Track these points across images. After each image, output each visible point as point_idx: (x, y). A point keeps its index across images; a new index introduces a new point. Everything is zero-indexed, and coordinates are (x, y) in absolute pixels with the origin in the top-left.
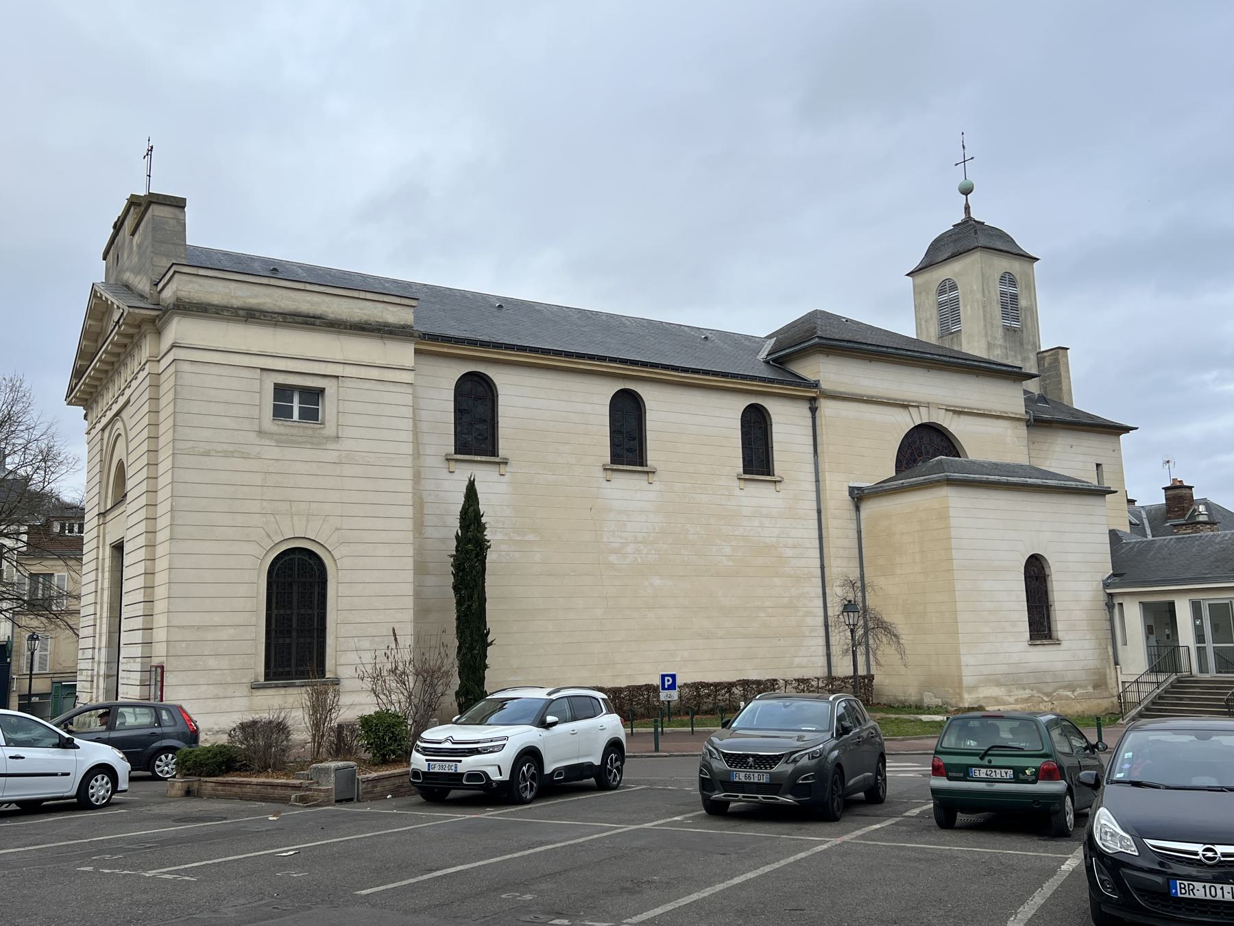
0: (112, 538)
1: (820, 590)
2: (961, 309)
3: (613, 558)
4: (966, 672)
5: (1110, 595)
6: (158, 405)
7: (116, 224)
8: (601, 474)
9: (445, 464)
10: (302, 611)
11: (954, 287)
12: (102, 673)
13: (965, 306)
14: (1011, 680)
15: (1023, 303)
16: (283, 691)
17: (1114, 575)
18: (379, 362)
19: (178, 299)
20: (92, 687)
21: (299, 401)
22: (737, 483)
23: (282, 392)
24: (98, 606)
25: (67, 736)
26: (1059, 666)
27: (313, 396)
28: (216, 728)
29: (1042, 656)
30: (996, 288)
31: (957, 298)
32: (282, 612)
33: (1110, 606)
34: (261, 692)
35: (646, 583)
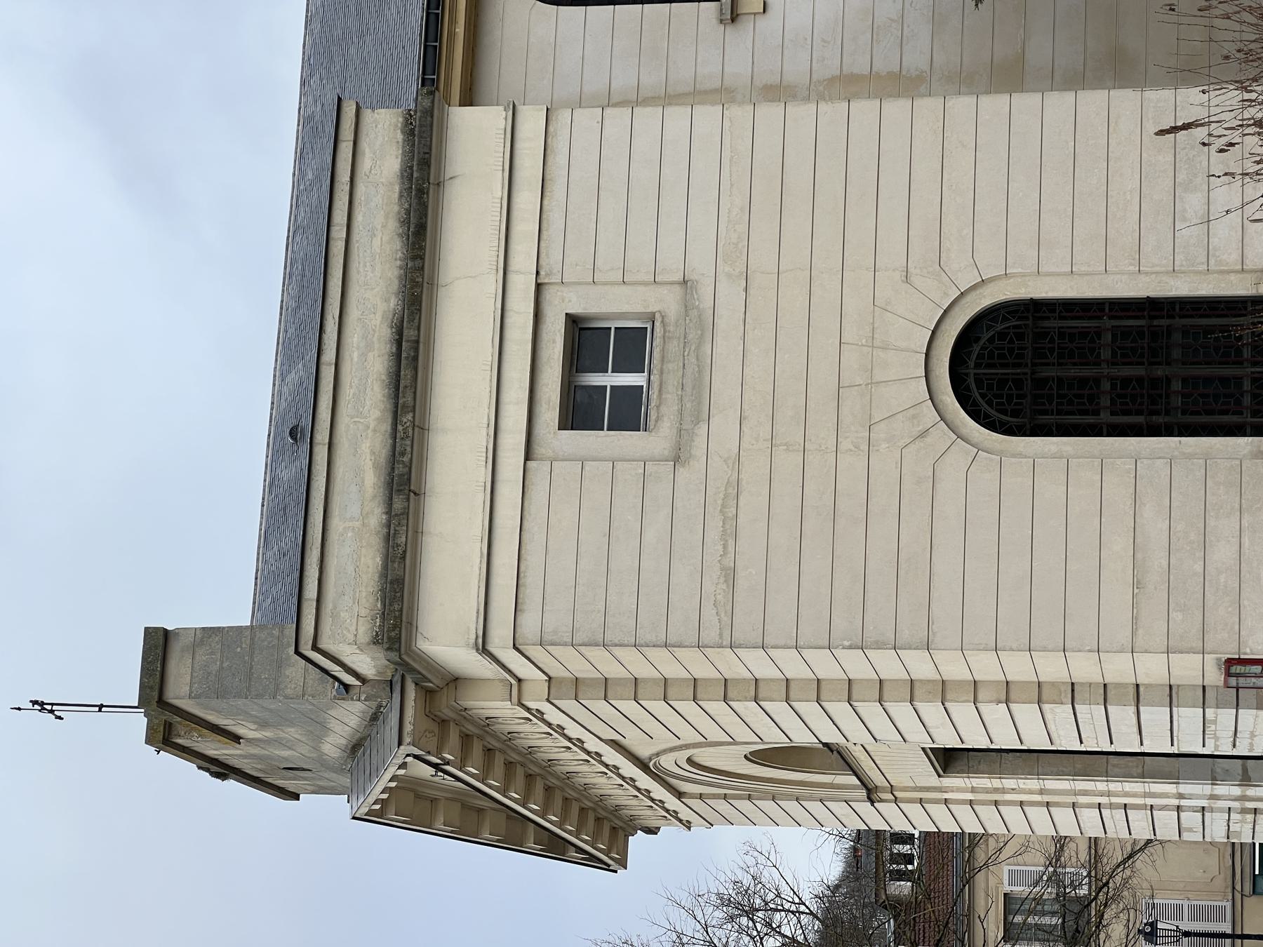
6: (619, 681)
9: (746, 25)
10: (1106, 354)
12: (1236, 791)
18: (499, 191)
19: (376, 641)
21: (599, 373)
23: (580, 411)
24: (1082, 800)
27: (586, 343)
32: (1105, 401)
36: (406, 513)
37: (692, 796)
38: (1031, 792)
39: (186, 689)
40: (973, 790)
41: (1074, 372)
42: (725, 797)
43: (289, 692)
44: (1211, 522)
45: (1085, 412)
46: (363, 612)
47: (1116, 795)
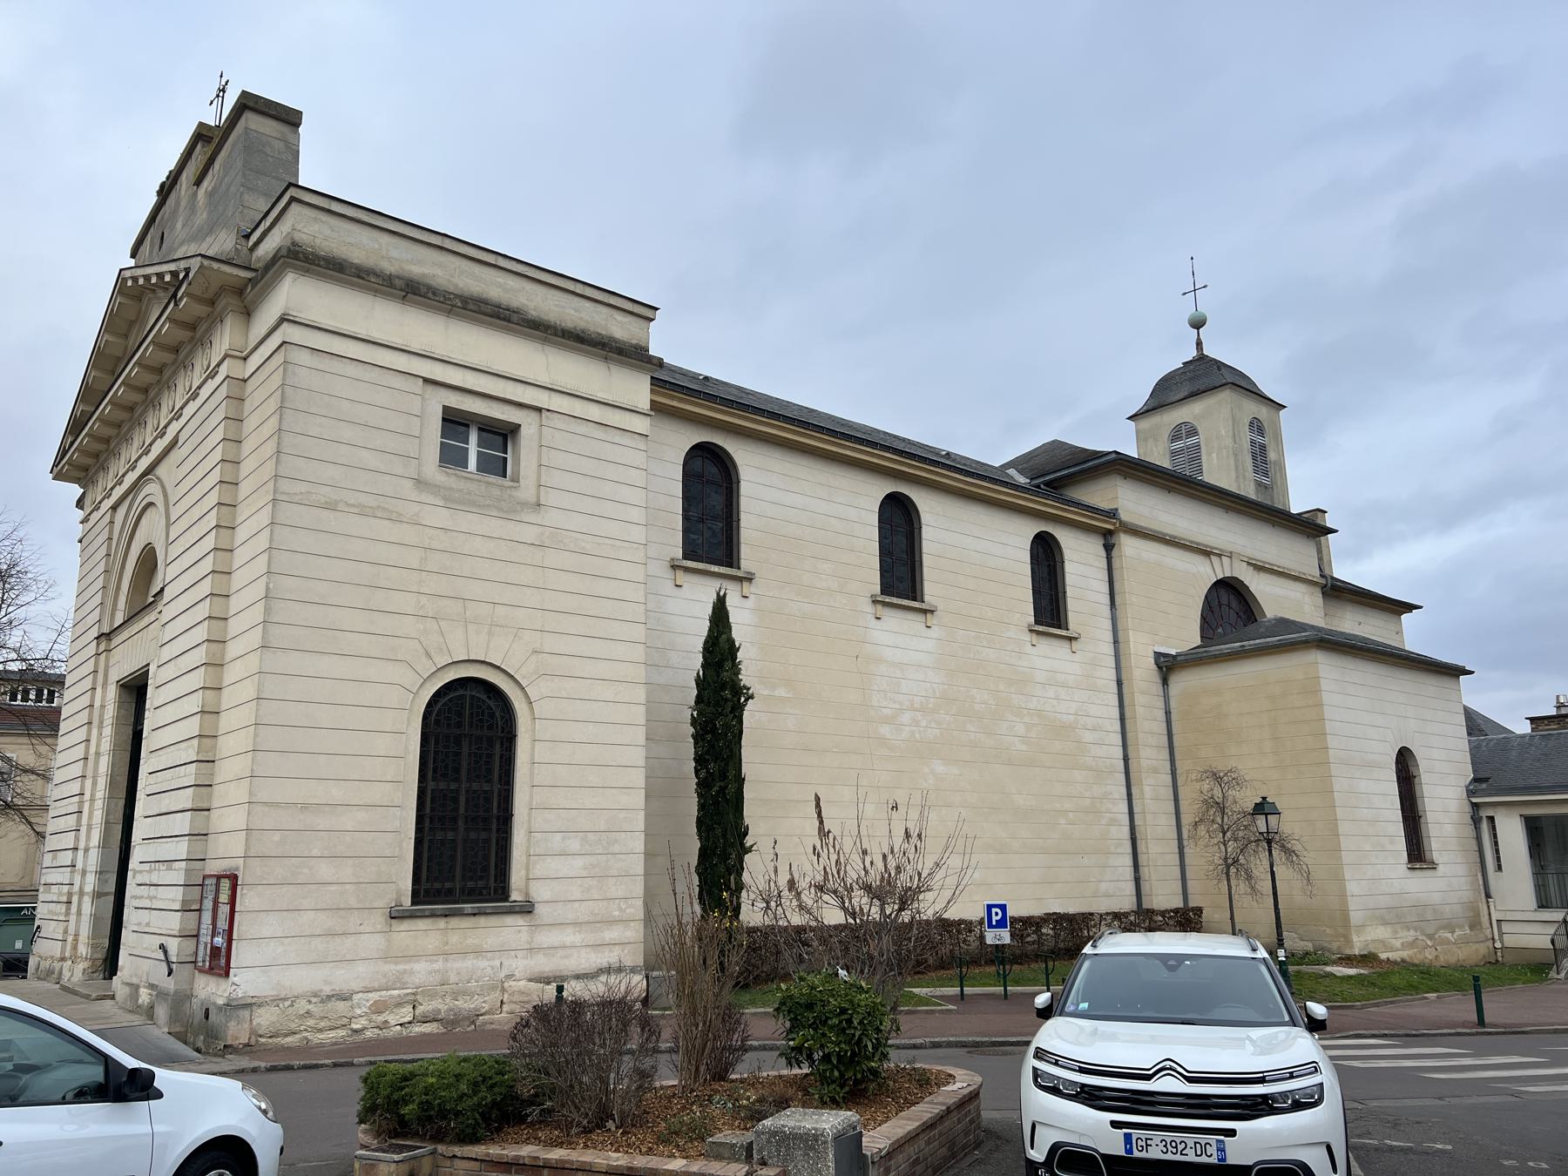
0: (123, 664)
1: (1124, 790)
2: (1204, 458)
3: (885, 730)
4: (1353, 904)
5: (1475, 806)
6: (240, 430)
7: (163, 185)
8: (869, 608)
9: (669, 574)
10: (475, 786)
11: (1193, 432)
12: (89, 888)
13: (1209, 454)
14: (1393, 916)
15: (1272, 456)
16: (442, 923)
17: (1475, 780)
18: (601, 396)
19: (294, 244)
20: (68, 913)
21: (481, 438)
22: (1027, 637)
23: (455, 422)
24: (88, 783)
25: (131, 1063)
26: (1436, 898)
27: (501, 435)
28: (327, 990)
29: (1420, 886)
30: (1246, 436)
31: (1198, 445)
32: (443, 785)
33: (1476, 821)
34: (406, 925)
35: (926, 770)
36: (392, 286)
37: (112, 516)
38: (98, 746)
39: (253, 127)
40: (103, 706)
41: (465, 764)
42: (110, 539)
43: (246, 197)
44: (350, 862)
45: (435, 771)
46: (318, 241)
47: (91, 805)
